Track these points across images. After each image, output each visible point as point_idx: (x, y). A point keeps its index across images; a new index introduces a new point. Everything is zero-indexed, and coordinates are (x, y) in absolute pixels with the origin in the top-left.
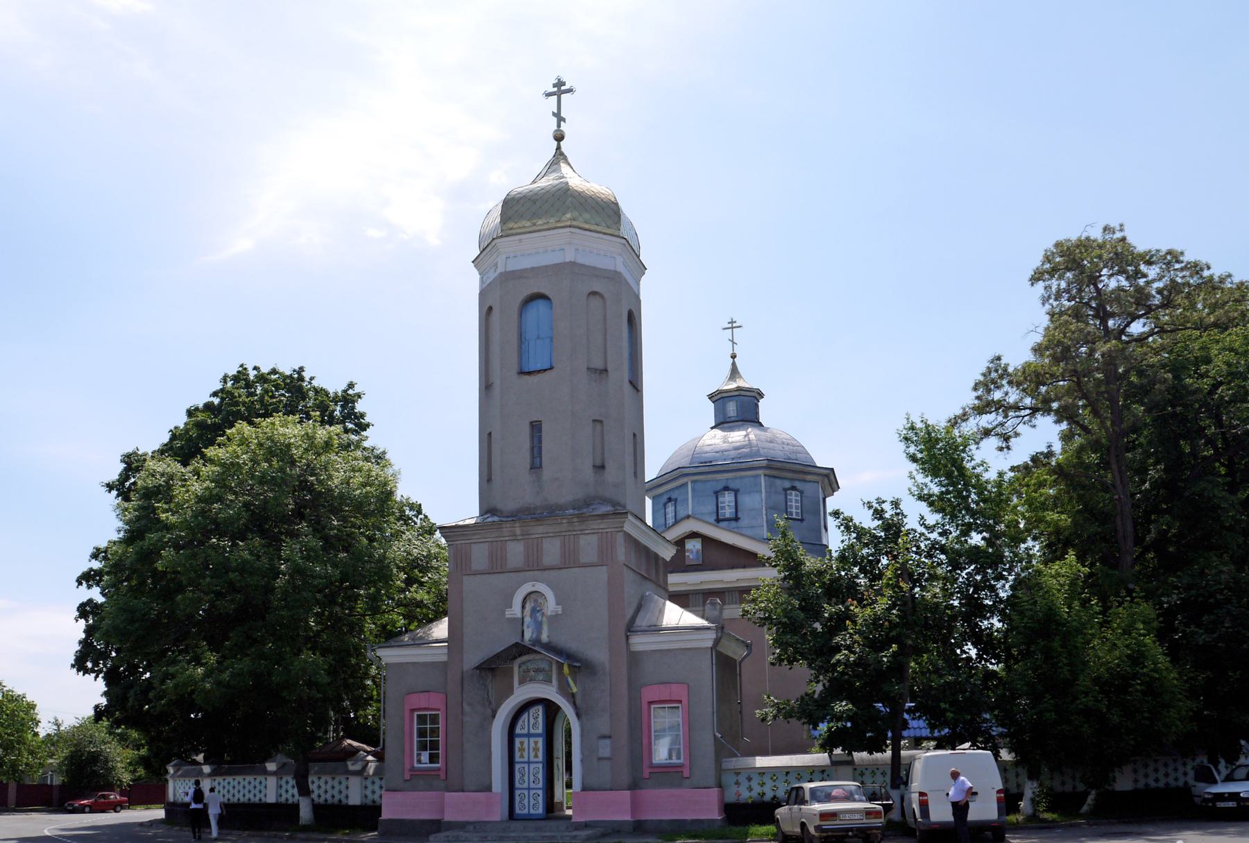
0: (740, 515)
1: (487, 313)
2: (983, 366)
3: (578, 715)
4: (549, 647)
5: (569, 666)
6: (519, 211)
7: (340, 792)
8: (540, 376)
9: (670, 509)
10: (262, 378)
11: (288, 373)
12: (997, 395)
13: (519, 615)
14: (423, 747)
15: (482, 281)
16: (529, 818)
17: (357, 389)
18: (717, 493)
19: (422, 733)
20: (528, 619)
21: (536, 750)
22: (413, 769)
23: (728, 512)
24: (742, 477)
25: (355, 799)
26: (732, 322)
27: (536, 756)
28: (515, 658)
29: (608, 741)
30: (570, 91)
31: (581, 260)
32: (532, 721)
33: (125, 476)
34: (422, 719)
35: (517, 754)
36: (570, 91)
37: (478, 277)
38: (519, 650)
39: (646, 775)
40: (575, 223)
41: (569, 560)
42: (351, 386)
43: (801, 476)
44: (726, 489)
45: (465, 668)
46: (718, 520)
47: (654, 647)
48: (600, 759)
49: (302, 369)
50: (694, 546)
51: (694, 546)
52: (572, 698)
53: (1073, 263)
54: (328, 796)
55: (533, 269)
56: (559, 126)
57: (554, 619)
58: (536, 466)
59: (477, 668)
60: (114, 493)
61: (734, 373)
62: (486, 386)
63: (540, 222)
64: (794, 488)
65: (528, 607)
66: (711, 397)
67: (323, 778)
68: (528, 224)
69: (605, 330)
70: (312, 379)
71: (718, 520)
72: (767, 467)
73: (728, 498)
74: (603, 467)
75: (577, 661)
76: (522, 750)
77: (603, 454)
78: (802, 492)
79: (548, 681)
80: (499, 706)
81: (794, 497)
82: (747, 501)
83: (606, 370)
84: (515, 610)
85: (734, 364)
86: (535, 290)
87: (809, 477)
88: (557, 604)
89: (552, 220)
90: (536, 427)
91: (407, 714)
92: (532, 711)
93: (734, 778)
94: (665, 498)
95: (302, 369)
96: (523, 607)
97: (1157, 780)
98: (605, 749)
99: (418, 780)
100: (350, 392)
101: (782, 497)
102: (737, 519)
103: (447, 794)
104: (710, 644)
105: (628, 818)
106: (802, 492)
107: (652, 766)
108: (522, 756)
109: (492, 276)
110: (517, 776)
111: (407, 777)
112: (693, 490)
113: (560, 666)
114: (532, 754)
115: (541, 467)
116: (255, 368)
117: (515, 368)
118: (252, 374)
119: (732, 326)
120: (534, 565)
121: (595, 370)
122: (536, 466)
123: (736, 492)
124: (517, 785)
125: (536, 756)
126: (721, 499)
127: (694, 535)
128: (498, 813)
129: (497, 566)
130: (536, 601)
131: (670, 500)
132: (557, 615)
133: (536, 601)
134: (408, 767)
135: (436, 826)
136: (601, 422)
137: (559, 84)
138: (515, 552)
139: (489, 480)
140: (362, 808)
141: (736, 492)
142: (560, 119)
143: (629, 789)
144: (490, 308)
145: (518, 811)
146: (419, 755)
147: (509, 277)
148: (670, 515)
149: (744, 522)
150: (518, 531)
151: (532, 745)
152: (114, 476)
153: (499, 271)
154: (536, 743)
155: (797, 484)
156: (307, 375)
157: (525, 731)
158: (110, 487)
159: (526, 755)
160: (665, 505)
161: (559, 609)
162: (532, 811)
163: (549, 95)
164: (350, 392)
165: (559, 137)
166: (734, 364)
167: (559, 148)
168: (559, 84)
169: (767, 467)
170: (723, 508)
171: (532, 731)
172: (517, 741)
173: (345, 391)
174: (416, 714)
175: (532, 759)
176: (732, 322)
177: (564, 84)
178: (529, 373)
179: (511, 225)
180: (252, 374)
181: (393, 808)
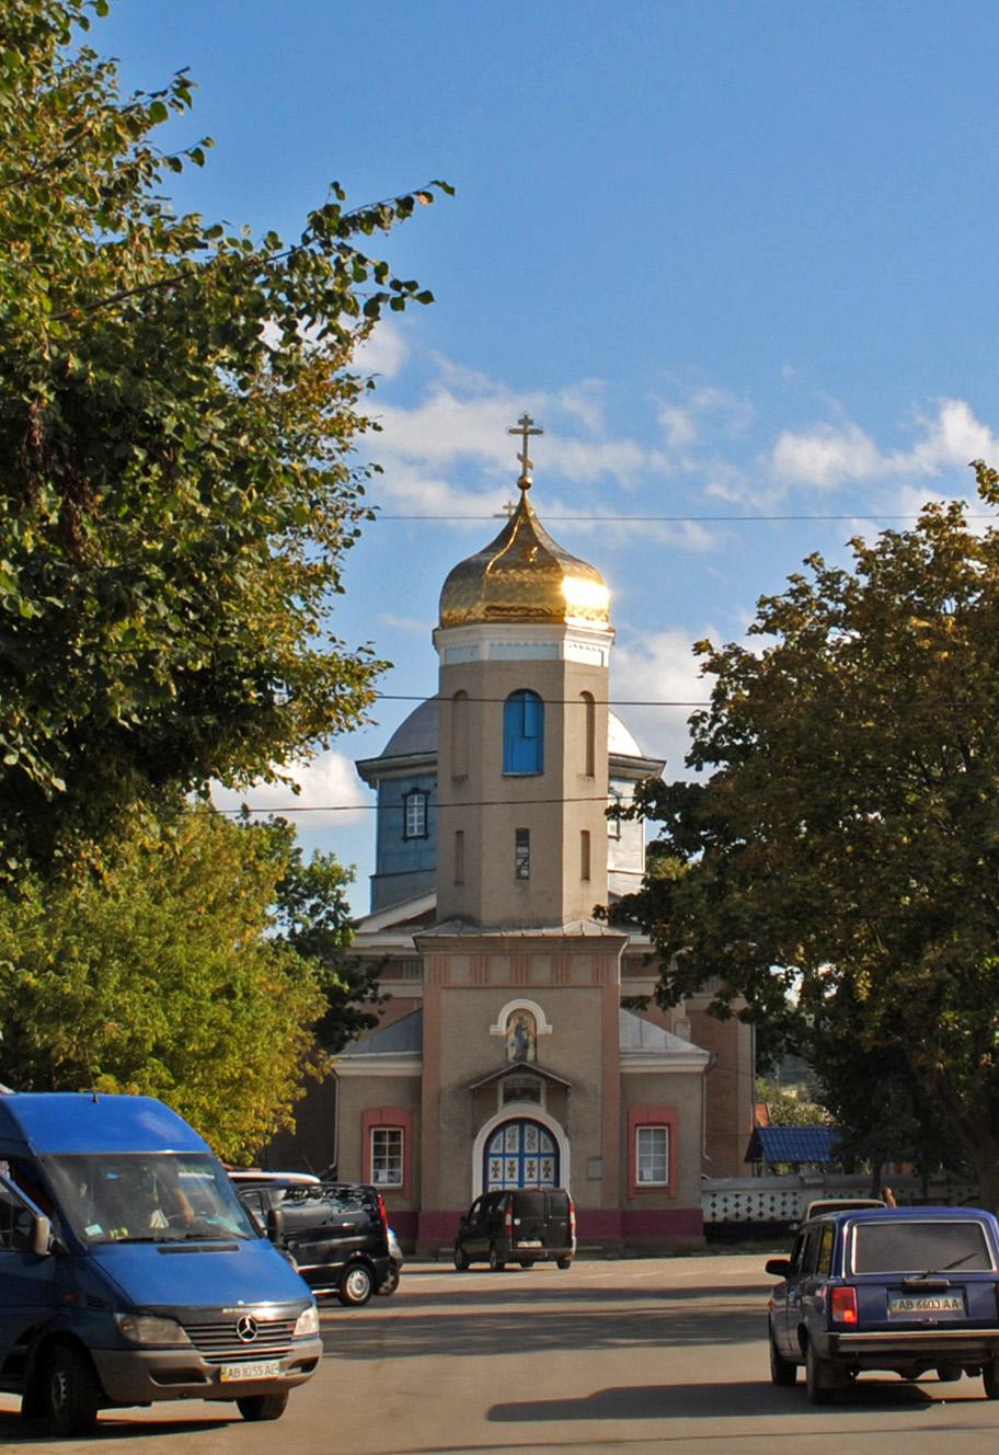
3: (567, 1135)
14: (379, 1163)
21: (531, 1169)
23: (415, 827)
27: (512, 1176)
29: (598, 1163)
32: (508, 1140)
34: (379, 1137)
35: (491, 1174)
36: (538, 432)
47: (645, 1070)
48: (589, 1179)
54: (742, 1210)
55: (522, 662)
71: (406, 839)
76: (496, 1170)
79: (535, 1098)
84: (501, 1027)
88: (548, 1022)
91: (366, 1129)
93: (711, 1200)
96: (508, 1024)
97: (772, 1209)
104: (701, 1069)
108: (496, 1176)
120: (521, 986)
123: (427, 793)
130: (521, 1018)
131: (416, 791)
133: (521, 1018)
137: (526, 421)
151: (507, 1165)
154: (512, 1163)
157: (500, 1151)
161: (550, 1029)
167: (523, 499)
168: (526, 421)
171: (507, 1151)
172: (491, 1161)
174: (373, 1130)
177: (531, 422)
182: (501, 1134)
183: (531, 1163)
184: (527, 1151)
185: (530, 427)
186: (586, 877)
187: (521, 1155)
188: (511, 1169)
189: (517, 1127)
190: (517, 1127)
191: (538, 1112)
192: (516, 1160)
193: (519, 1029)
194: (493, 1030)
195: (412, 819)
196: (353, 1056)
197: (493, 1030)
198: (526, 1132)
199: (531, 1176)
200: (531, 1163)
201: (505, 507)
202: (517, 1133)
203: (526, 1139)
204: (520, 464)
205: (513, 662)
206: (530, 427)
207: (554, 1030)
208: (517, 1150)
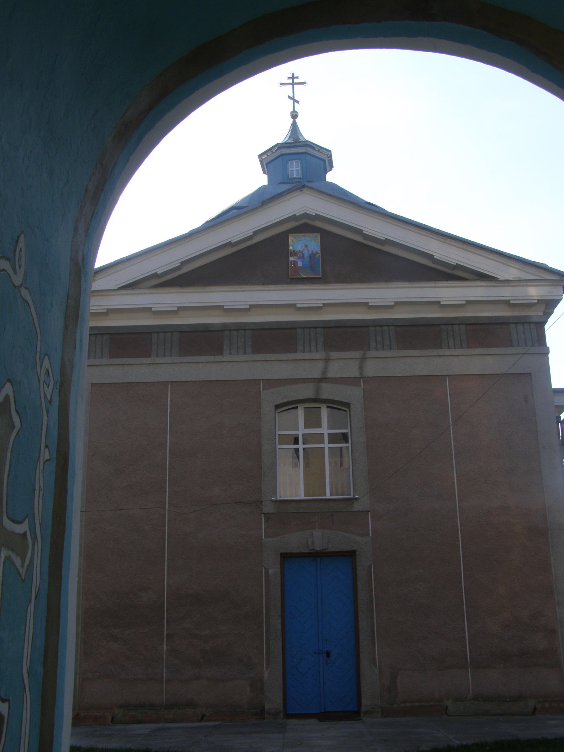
26: (293, 78)
176: (293, 78)
201: (289, 78)
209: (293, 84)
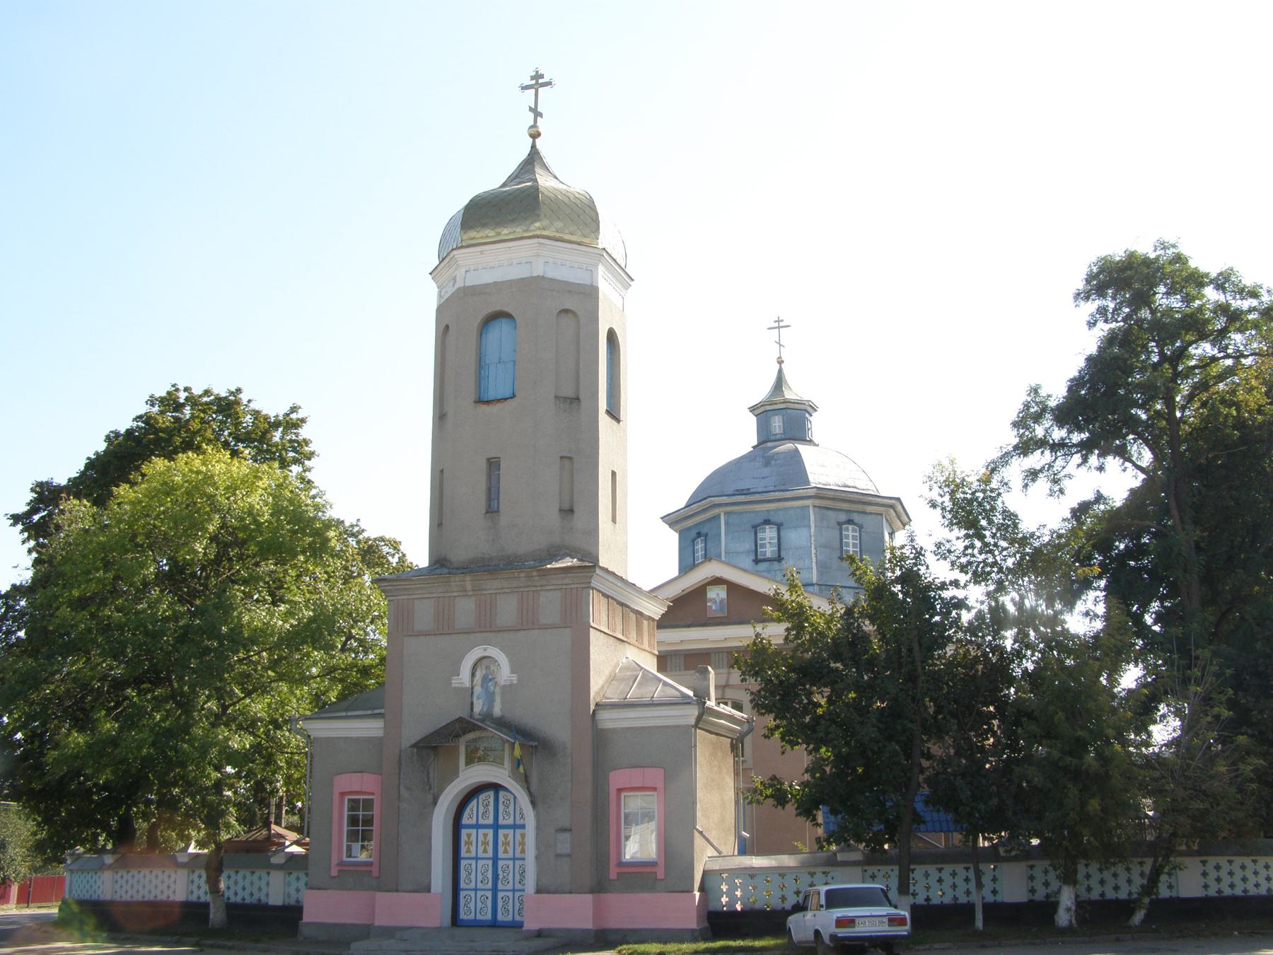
0: (783, 554)
1: (444, 333)
2: (1022, 397)
3: (533, 803)
4: (503, 724)
5: (522, 746)
6: (488, 214)
7: (260, 889)
8: (499, 405)
9: (700, 546)
10: (192, 401)
11: (223, 394)
12: (1039, 432)
13: (468, 684)
15: (440, 296)
16: (476, 925)
17: (301, 414)
18: (755, 528)
19: (353, 821)
20: (478, 690)
21: (485, 843)
22: (341, 864)
23: (769, 551)
24: (786, 509)
25: (276, 899)
27: (485, 851)
28: (458, 736)
29: (568, 835)
30: (549, 84)
31: (552, 273)
32: (481, 810)
33: (34, 508)
34: (354, 805)
35: (463, 849)
36: (549, 84)
37: (436, 290)
38: (463, 726)
39: (613, 876)
40: (545, 233)
41: (528, 621)
42: (294, 409)
43: (860, 507)
44: (767, 522)
45: (403, 747)
46: (757, 561)
48: (558, 856)
49: (239, 390)
50: (717, 594)
51: (717, 594)
52: (526, 781)
53: (1123, 279)
56: (535, 121)
57: (508, 689)
58: (492, 510)
59: (414, 746)
60: (20, 527)
61: (780, 383)
62: (441, 416)
63: (505, 231)
64: (850, 522)
65: (479, 675)
66: (752, 409)
67: (257, 874)
68: (492, 233)
69: (578, 352)
70: (249, 401)
71: (757, 561)
72: (816, 497)
73: (769, 534)
74: (572, 511)
75: (533, 739)
76: (469, 843)
77: (572, 497)
78: (861, 527)
80: (441, 791)
81: (850, 532)
82: (794, 537)
83: (578, 399)
84: (464, 678)
85: (780, 371)
86: (498, 308)
87: (869, 509)
88: (512, 672)
89: (519, 230)
90: (493, 465)
91: (336, 797)
92: (482, 797)
94: (694, 533)
95: (239, 390)
96: (473, 675)
97: (1116, 888)
98: (564, 844)
99: (354, 877)
100: (294, 416)
101: (836, 533)
102: (779, 559)
103: (378, 894)
105: (589, 925)
106: (861, 527)
107: (621, 864)
108: (469, 851)
109: (450, 290)
110: (463, 874)
111: (334, 872)
112: (727, 523)
113: (512, 746)
114: (481, 848)
115: (498, 511)
116: (186, 389)
117: (473, 397)
118: (182, 396)
119: (779, 325)
120: (486, 627)
121: (565, 398)
122: (492, 510)
124: (462, 885)
125: (485, 851)
126: (760, 535)
127: (717, 581)
128: (438, 914)
129: (444, 626)
130: (487, 668)
131: (699, 535)
132: (511, 685)
133: (487, 668)
134: (335, 861)
135: (365, 932)
136: (571, 458)
137: (537, 76)
138: (465, 610)
139: (440, 525)
140: (285, 909)
141: (779, 527)
142: (537, 113)
143: (592, 891)
144: (447, 327)
145: (462, 916)
146: (349, 848)
147: (468, 293)
148: (700, 554)
149: (790, 564)
150: (469, 586)
151: (481, 838)
152: (22, 508)
153: (457, 286)
154: (485, 835)
155: (856, 517)
156: (244, 397)
158: (16, 519)
159: (473, 848)
160: (693, 541)
162: (479, 917)
163: (524, 88)
164: (294, 416)
165: (535, 135)
166: (780, 371)
167: (533, 146)
168: (537, 76)
169: (816, 497)
170: (763, 546)
171: (481, 821)
172: (464, 832)
173: (287, 415)
174: (347, 798)
175: (480, 854)
176: (779, 321)
178: (488, 402)
179: (472, 234)
180: (182, 396)
181: (323, 908)
182: (474, 802)
183: (506, 836)
184: (501, 822)
185: (541, 81)
186: (614, 520)
187: (496, 827)
188: (485, 843)
189: (492, 794)
190: (492, 794)
191: (471, 775)
192: (490, 832)
193: (486, 680)
194: (455, 682)
195: (847, 537)
196: (350, 714)
197: (455, 682)
198: (501, 800)
199: (506, 851)
200: (506, 836)
202: (492, 800)
203: (501, 808)
204: (532, 115)
205: (487, 285)
206: (541, 81)
207: (519, 679)
208: (490, 821)
209: (779, 327)
